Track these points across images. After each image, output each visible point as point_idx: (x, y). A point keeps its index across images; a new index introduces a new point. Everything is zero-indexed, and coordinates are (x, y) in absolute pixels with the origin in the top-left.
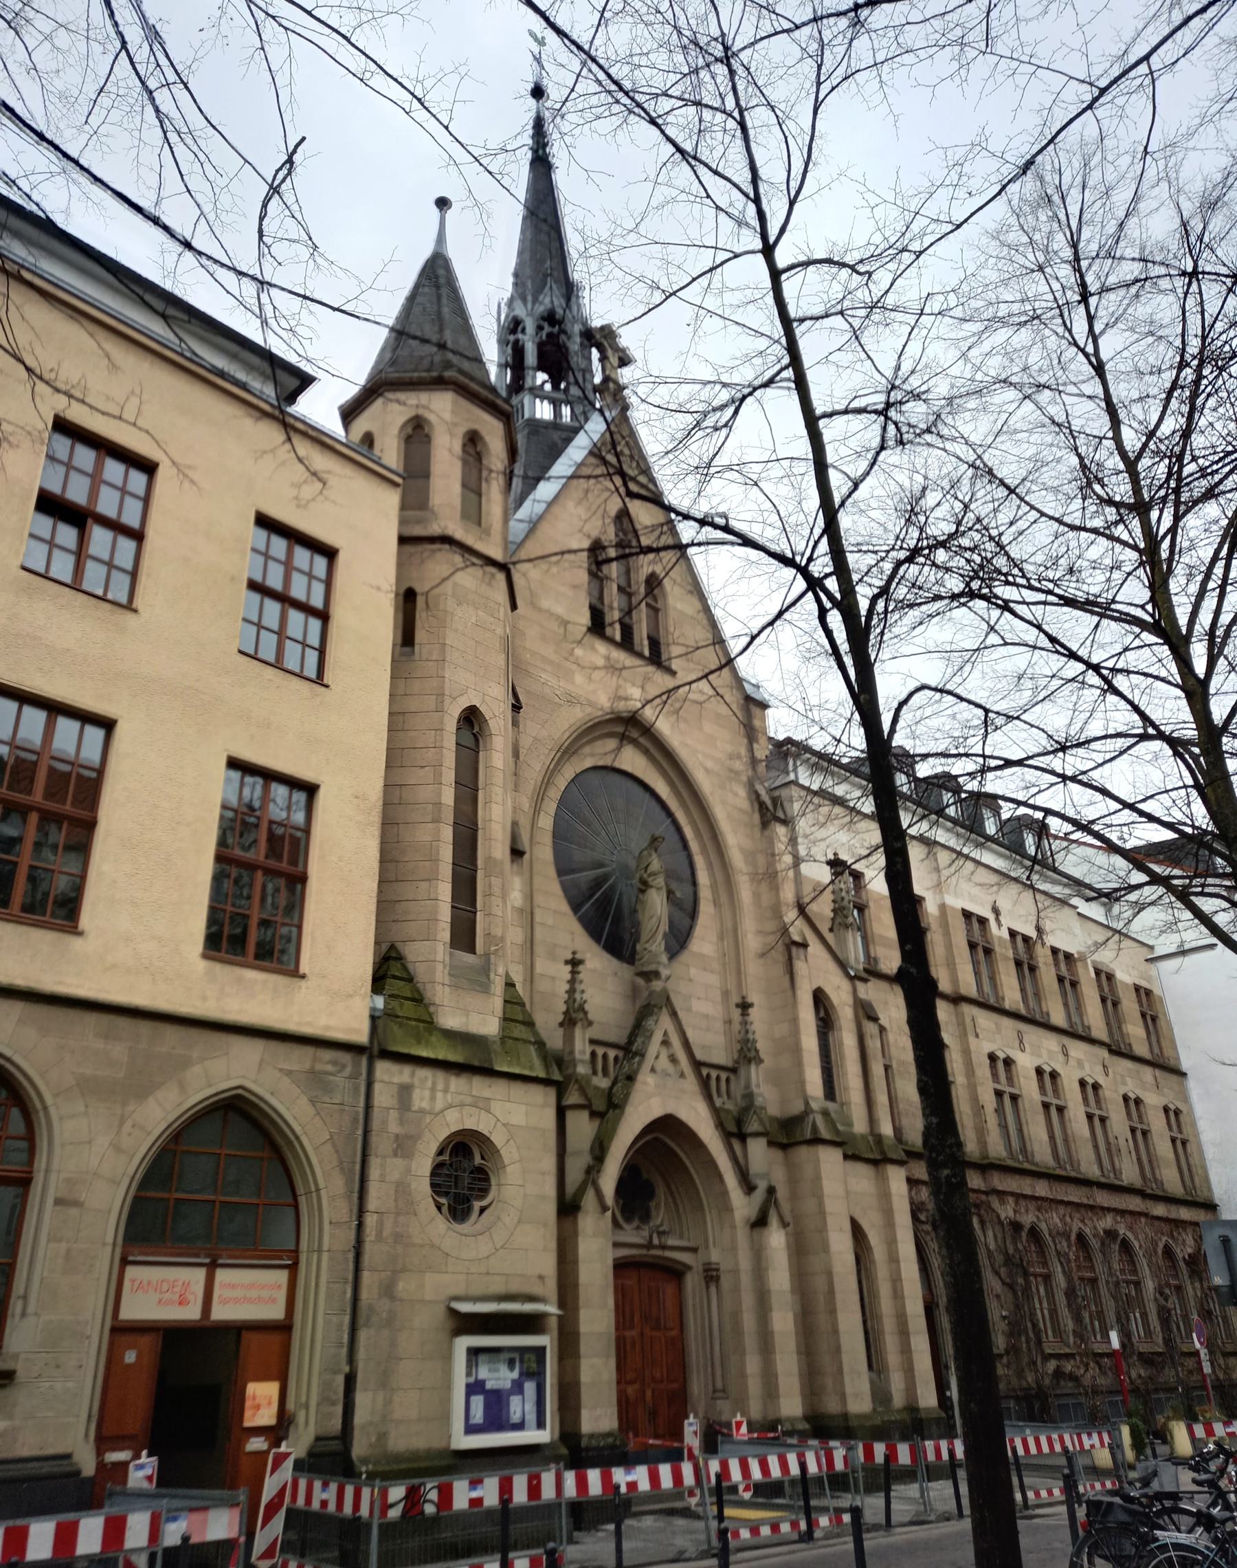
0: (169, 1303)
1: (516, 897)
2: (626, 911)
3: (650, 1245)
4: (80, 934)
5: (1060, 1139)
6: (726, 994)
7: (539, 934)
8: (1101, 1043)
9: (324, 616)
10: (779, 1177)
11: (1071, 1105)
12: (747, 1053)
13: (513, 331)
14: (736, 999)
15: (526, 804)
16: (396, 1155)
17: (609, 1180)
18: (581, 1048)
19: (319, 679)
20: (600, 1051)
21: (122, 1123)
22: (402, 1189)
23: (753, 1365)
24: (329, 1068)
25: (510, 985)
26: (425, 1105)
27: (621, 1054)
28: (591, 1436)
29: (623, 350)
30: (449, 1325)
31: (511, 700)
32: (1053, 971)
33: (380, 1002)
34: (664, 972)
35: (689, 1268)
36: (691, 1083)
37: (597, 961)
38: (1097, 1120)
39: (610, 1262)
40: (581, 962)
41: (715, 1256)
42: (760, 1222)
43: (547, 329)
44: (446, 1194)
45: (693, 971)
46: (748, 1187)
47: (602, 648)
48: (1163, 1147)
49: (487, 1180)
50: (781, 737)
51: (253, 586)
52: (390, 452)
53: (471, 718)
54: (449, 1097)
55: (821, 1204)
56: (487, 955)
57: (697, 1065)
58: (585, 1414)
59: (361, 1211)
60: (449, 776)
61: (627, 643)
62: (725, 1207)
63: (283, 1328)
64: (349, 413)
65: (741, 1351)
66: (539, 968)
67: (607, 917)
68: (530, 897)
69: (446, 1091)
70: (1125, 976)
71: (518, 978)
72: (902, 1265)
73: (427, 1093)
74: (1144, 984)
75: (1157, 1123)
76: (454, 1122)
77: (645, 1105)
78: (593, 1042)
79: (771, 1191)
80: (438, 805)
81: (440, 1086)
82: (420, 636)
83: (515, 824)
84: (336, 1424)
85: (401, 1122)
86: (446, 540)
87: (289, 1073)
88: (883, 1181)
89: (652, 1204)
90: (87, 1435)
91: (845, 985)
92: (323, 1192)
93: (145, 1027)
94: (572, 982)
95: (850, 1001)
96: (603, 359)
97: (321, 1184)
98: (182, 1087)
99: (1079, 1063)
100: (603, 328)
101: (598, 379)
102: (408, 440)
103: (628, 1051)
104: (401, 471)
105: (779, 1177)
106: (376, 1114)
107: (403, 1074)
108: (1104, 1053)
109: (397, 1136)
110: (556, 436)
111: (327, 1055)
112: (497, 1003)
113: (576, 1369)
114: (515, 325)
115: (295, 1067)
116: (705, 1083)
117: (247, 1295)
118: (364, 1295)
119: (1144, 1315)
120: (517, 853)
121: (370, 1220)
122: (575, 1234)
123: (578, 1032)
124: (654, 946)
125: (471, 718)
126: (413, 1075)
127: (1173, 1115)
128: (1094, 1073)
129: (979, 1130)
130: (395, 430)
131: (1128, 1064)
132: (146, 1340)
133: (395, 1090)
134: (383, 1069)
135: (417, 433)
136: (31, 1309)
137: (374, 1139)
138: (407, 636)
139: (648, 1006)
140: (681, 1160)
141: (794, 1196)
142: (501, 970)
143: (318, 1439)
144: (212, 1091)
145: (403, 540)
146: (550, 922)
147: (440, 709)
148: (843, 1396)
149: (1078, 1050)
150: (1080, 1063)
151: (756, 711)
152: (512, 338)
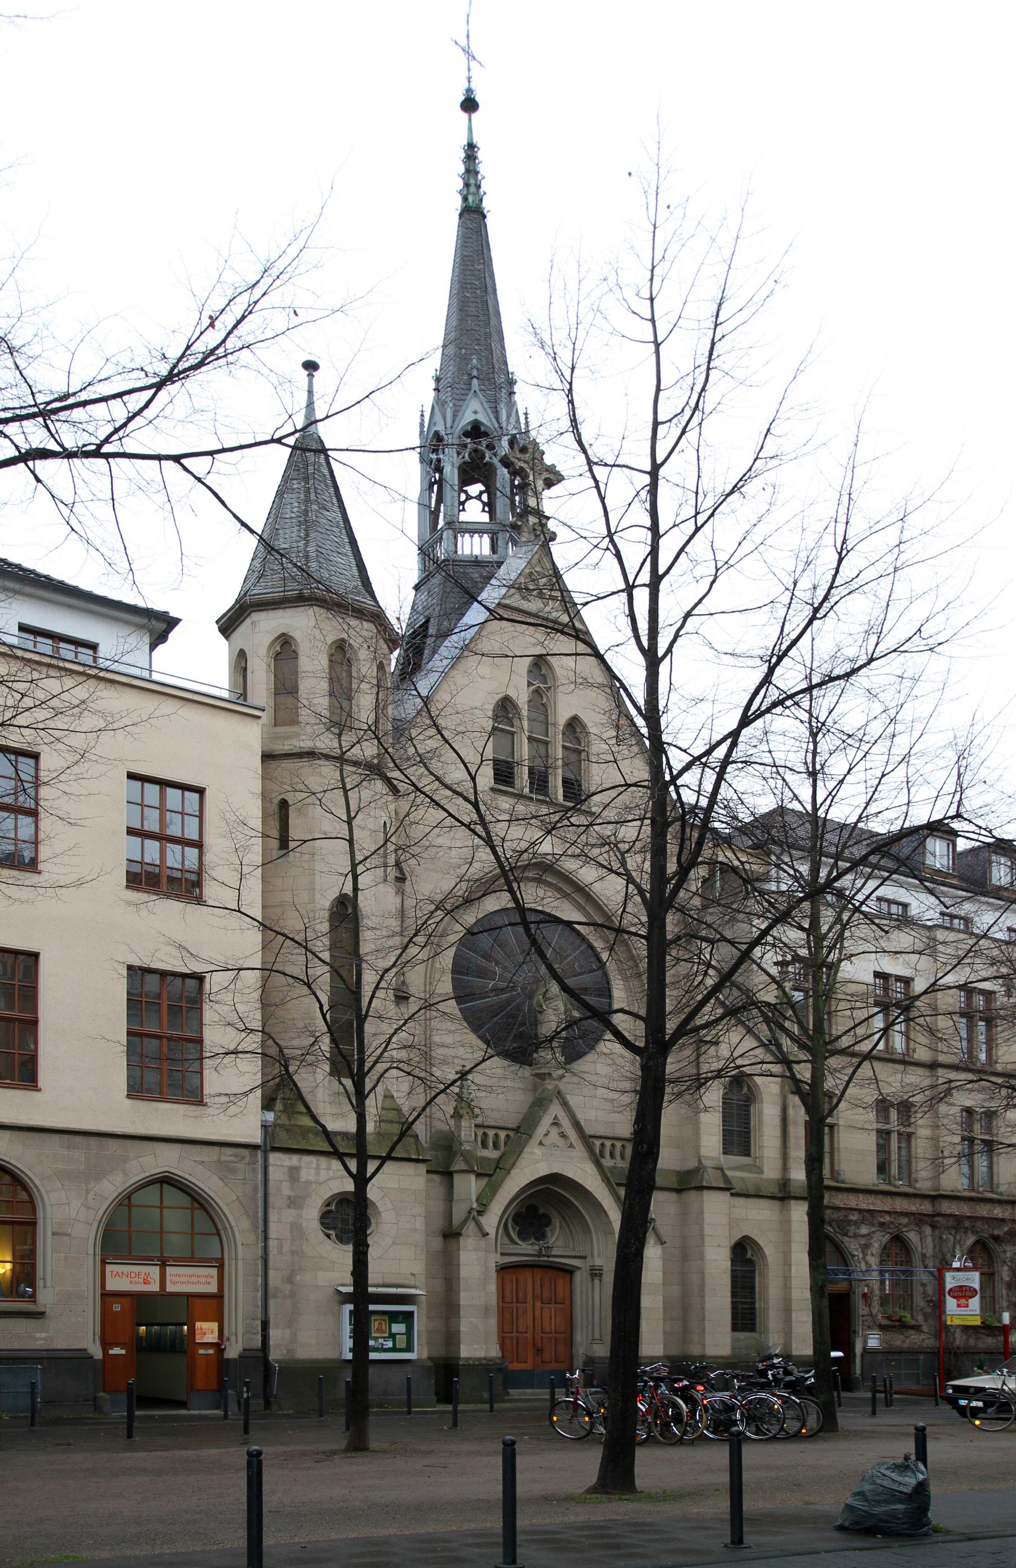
4: (40, 1090)
16: (289, 1207)
21: (87, 1192)
22: (297, 1230)
24: (232, 1159)
26: (311, 1178)
27: (512, 1134)
30: (338, 1298)
33: (270, 1116)
35: (579, 1268)
36: (580, 1151)
39: (492, 1265)
44: (334, 1229)
51: (131, 832)
54: (331, 1173)
55: (702, 1229)
57: (586, 1139)
58: (463, 1347)
59: (266, 1239)
69: (328, 1169)
72: (793, 1268)
73: (313, 1171)
77: (533, 1165)
78: (476, 1126)
84: (257, 1342)
85: (292, 1189)
89: (548, 1230)
90: (94, 1342)
92: (235, 1229)
93: (93, 1141)
97: (233, 1224)
101: (396, 653)
102: (277, 657)
106: (271, 1184)
107: (294, 1160)
109: (289, 1197)
110: (475, 574)
111: (230, 1151)
115: (206, 1159)
117: (189, 1280)
118: (271, 1282)
121: (272, 1244)
126: (300, 1160)
130: (263, 651)
132: (126, 1301)
133: (287, 1169)
134: (274, 1158)
135: (285, 648)
136: (49, 1284)
137: (271, 1199)
140: (573, 1203)
143: (244, 1350)
148: (704, 1346)
152: (434, 456)
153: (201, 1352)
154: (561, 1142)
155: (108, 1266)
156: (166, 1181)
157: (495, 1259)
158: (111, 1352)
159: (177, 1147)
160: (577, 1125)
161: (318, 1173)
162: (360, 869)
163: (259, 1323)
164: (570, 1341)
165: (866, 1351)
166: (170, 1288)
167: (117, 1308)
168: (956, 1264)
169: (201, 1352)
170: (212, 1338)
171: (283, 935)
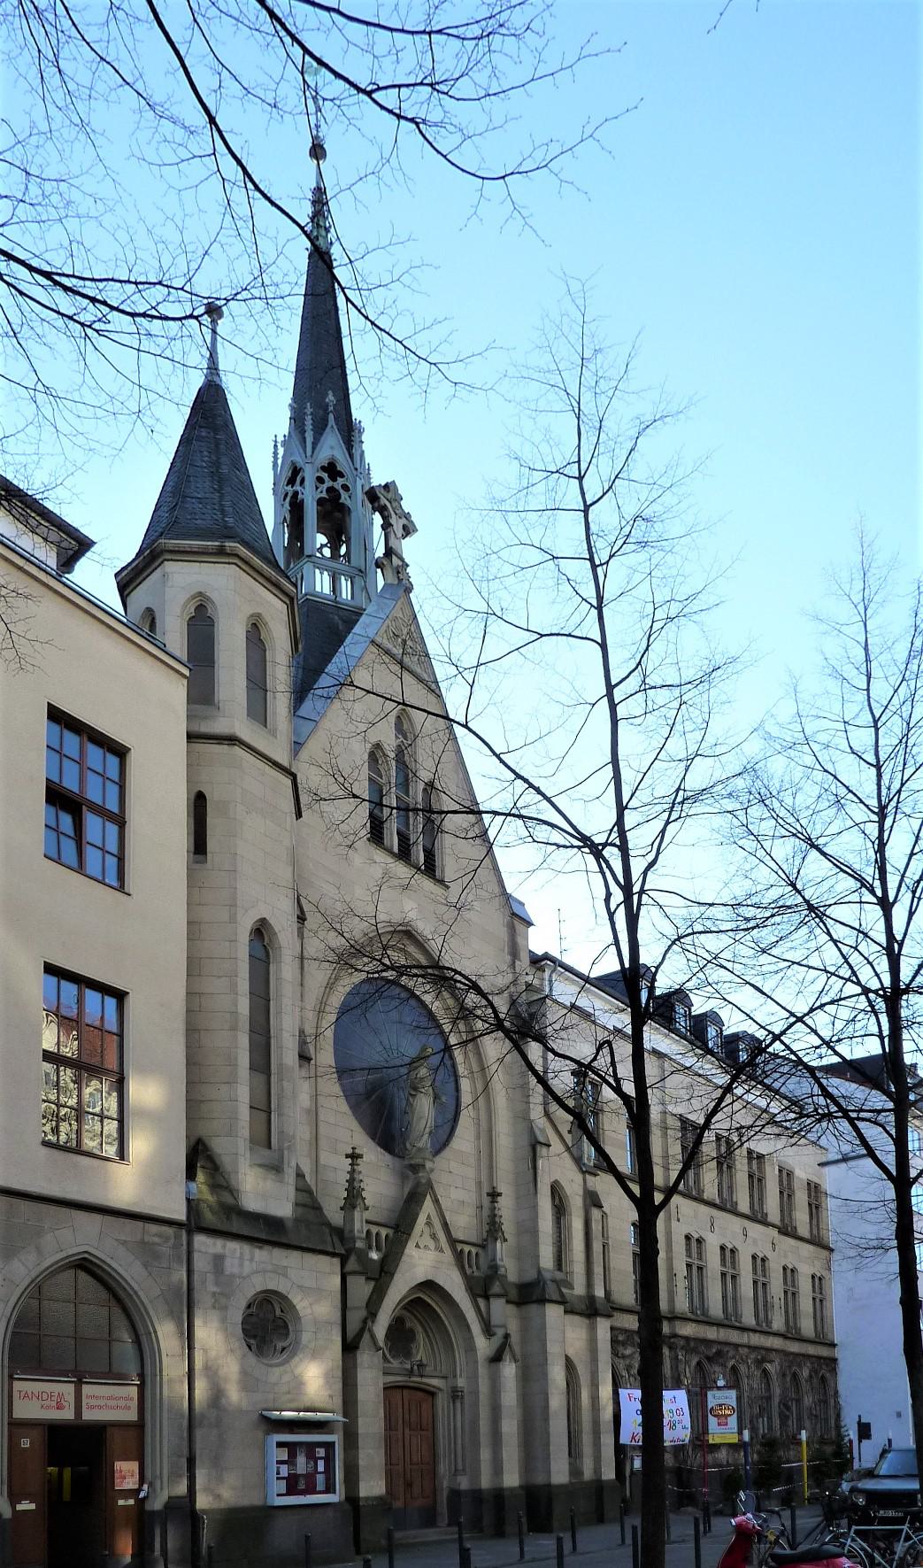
0: (49, 1407)
1: (304, 1099)
2: (398, 1113)
3: (411, 1373)
5: (731, 1299)
6: (479, 1184)
7: (322, 1130)
8: (774, 1226)
9: (120, 821)
10: (513, 1327)
11: (743, 1273)
12: (493, 1229)
13: (291, 481)
14: (486, 1189)
15: (311, 1015)
17: (381, 1328)
18: (359, 1227)
19: (121, 887)
20: (374, 1230)
23: (485, 1455)
24: (156, 1239)
25: (300, 1175)
26: (236, 1270)
28: (367, 1498)
29: (407, 516)
31: (297, 912)
32: (746, 1168)
34: (428, 1165)
36: (448, 1255)
37: (373, 1155)
38: (761, 1286)
40: (360, 1156)
41: (461, 1382)
42: (496, 1358)
43: (328, 483)
44: (254, 1337)
45: (453, 1164)
46: (488, 1331)
47: (380, 856)
48: (806, 1304)
49: (286, 1327)
50: (540, 952)
52: (175, 634)
53: (261, 931)
56: (281, 1150)
57: (453, 1242)
58: (362, 1485)
59: (191, 1348)
60: (244, 985)
61: (404, 854)
62: (471, 1348)
63: (139, 1426)
64: (128, 581)
65: (476, 1445)
66: (322, 1160)
67: (382, 1116)
68: (315, 1096)
69: (251, 1260)
70: (801, 1174)
71: (307, 1169)
74: (815, 1180)
75: (805, 1286)
76: (258, 1284)
78: (368, 1222)
79: (507, 1336)
80: (235, 1013)
81: (247, 1256)
82: (211, 844)
83: (302, 1032)
85: (217, 1284)
86: (232, 740)
87: (124, 1243)
88: (592, 1329)
91: (578, 1177)
94: (352, 1172)
95: (581, 1192)
96: (386, 526)
98: (39, 1250)
99: (758, 1239)
100: (386, 487)
101: (380, 552)
103: (401, 1225)
104: (185, 658)
105: (513, 1327)
108: (775, 1232)
112: (290, 1191)
113: (356, 1458)
114: (295, 475)
116: (459, 1256)
117: (108, 1403)
119: (770, 1419)
120: (304, 1058)
122: (355, 1366)
123: (357, 1214)
124: (422, 1140)
125: (261, 931)
127: (818, 1281)
128: (764, 1250)
129: (674, 1294)
131: (792, 1242)
134: (200, 1240)
135: (201, 623)
138: (199, 846)
139: (414, 1197)
141: (524, 1341)
142: (293, 1164)
144: (64, 1254)
145: (192, 737)
146: (332, 1120)
147: (233, 919)
149: (755, 1230)
150: (755, 1242)
151: (519, 926)
153: (121, 1502)
154: (431, 1244)
155: (16, 1384)
156: (85, 1265)
157: (382, 1381)
158: (19, 1507)
159: (97, 1218)
160: (445, 1225)
161: (241, 1265)
162: (618, 694)
163: (184, 1461)
164: (434, 1473)
165: (632, 1472)
166: (88, 1415)
167: (25, 1443)
168: (721, 1383)
169: (121, 1502)
170: (131, 1483)
171: (526, 781)
